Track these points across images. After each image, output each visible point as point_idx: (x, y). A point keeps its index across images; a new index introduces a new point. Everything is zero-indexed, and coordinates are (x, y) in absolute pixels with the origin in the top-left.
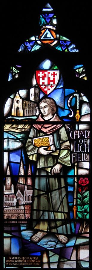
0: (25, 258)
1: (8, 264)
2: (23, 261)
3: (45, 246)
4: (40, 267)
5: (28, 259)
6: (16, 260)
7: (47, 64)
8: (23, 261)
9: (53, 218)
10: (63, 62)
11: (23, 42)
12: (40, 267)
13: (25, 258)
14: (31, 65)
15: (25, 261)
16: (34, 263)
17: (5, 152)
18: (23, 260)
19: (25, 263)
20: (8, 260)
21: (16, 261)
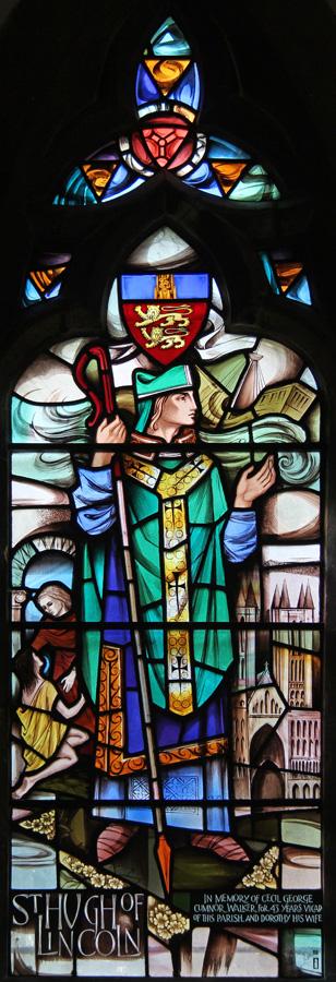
0: (265, 898)
1: (201, 918)
2: (256, 908)
3: (37, 852)
4: (50, 934)
5: (276, 903)
6: (231, 903)
7: (164, 249)
8: (256, 908)
9: (291, 797)
10: (221, 241)
11: (321, 400)
12: (50, 934)
13: (265, 898)
14: (108, 243)
15: (265, 909)
16: (297, 913)
17: (197, 629)
18: (254, 904)
19: (265, 913)
20: (201, 903)
21: (230, 908)
